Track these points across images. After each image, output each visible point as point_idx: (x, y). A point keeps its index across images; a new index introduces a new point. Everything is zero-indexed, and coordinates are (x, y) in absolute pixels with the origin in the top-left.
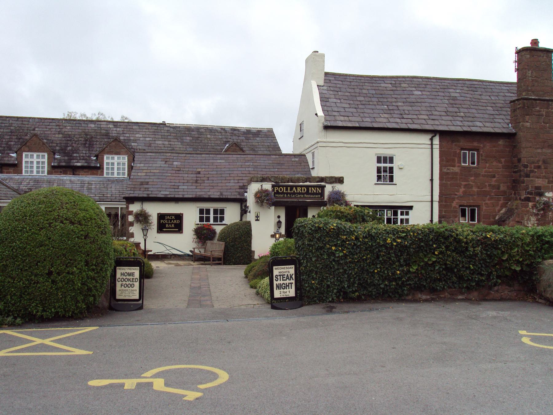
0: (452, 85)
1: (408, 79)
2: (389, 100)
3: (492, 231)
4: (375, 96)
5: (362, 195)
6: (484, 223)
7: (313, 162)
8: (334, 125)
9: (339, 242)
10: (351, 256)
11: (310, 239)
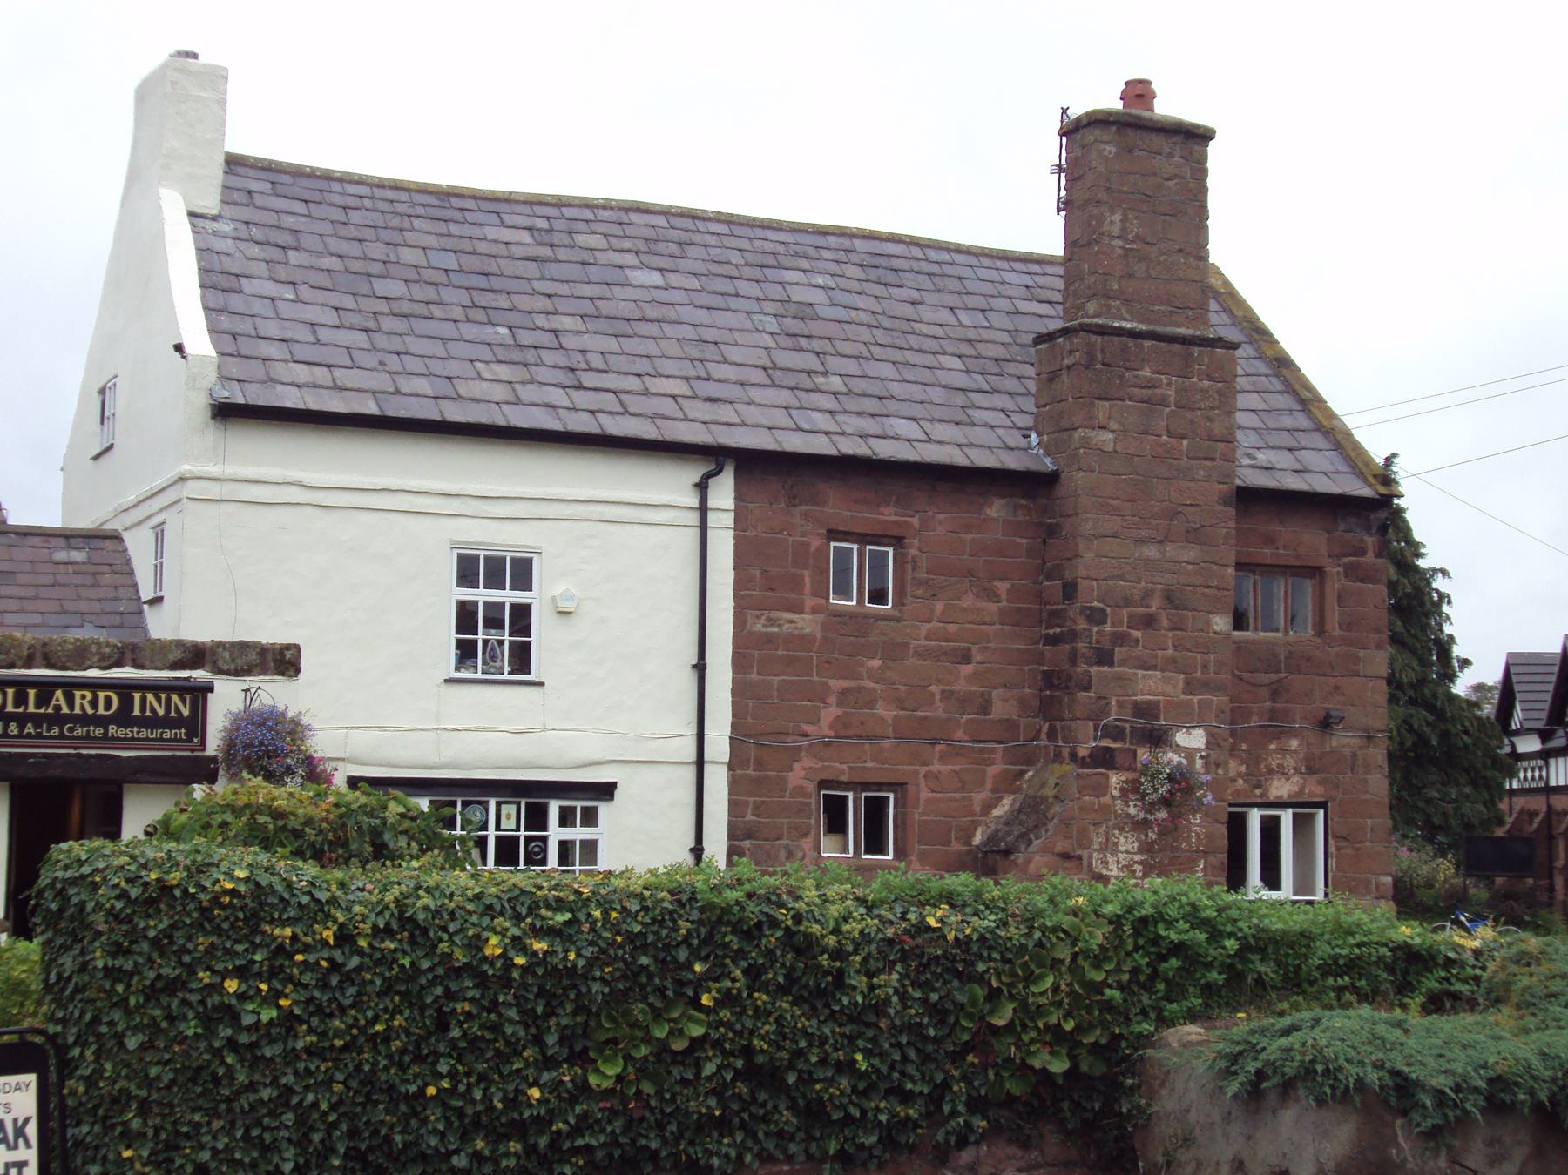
0: (796, 254)
1: (605, 214)
2: (519, 300)
3: (950, 899)
4: (456, 278)
5: (383, 728)
6: (924, 858)
7: (158, 570)
8: (261, 403)
9: (258, 957)
10: (315, 1021)
11: (118, 944)
